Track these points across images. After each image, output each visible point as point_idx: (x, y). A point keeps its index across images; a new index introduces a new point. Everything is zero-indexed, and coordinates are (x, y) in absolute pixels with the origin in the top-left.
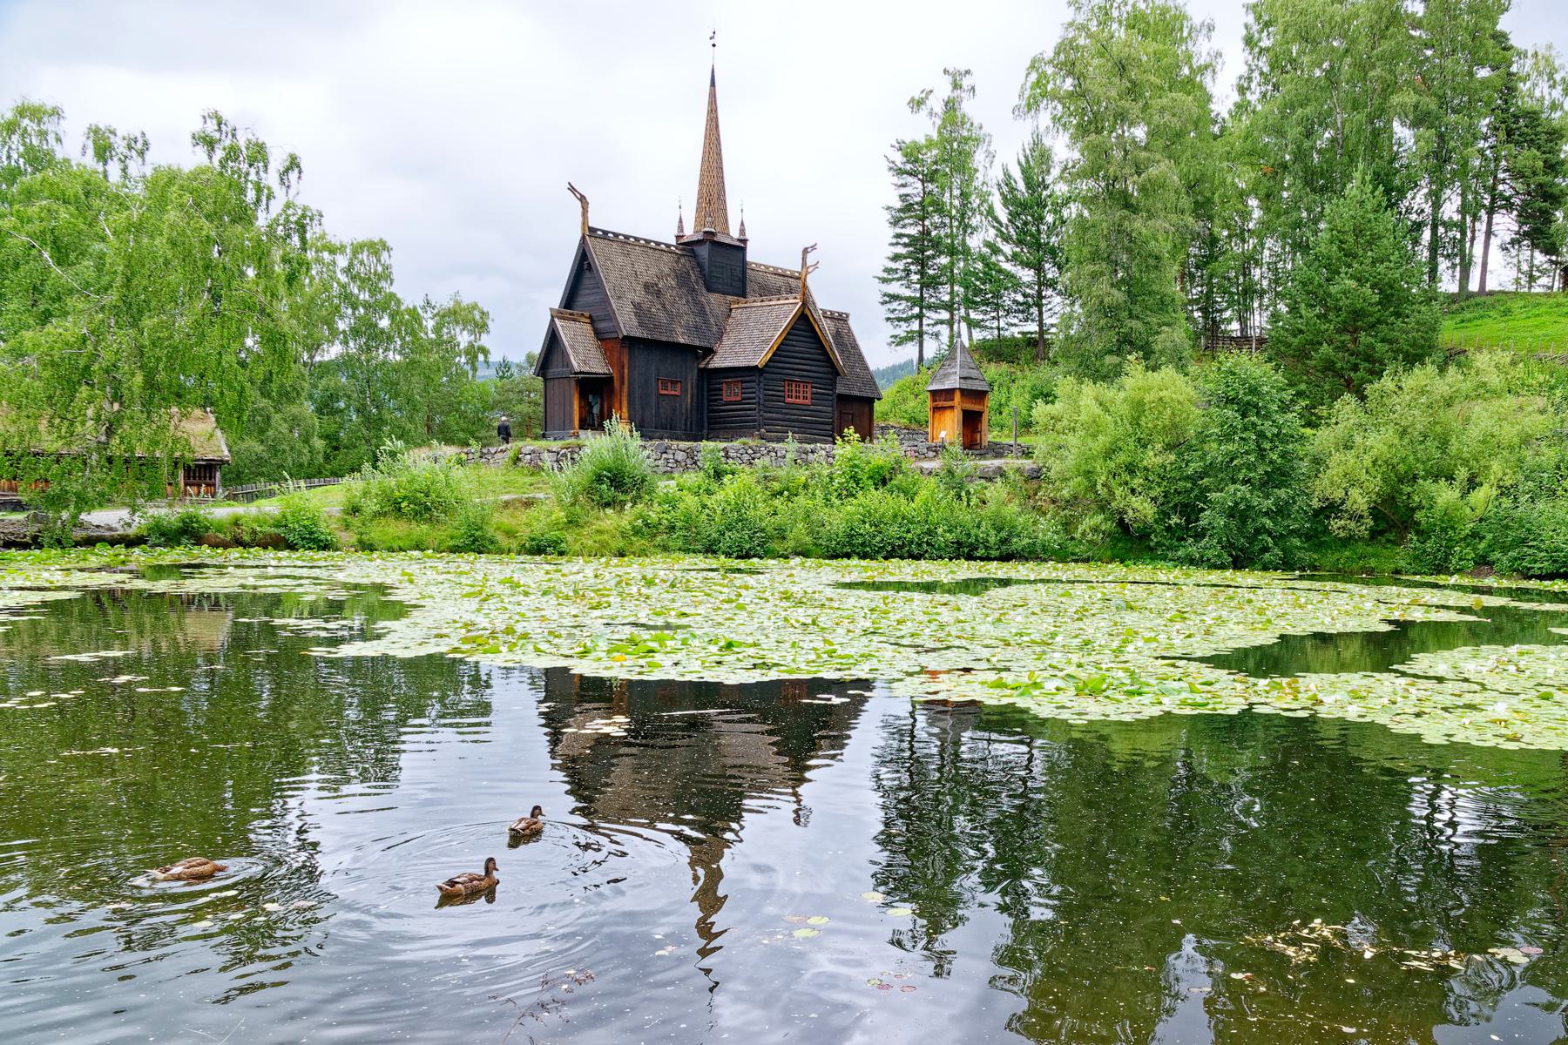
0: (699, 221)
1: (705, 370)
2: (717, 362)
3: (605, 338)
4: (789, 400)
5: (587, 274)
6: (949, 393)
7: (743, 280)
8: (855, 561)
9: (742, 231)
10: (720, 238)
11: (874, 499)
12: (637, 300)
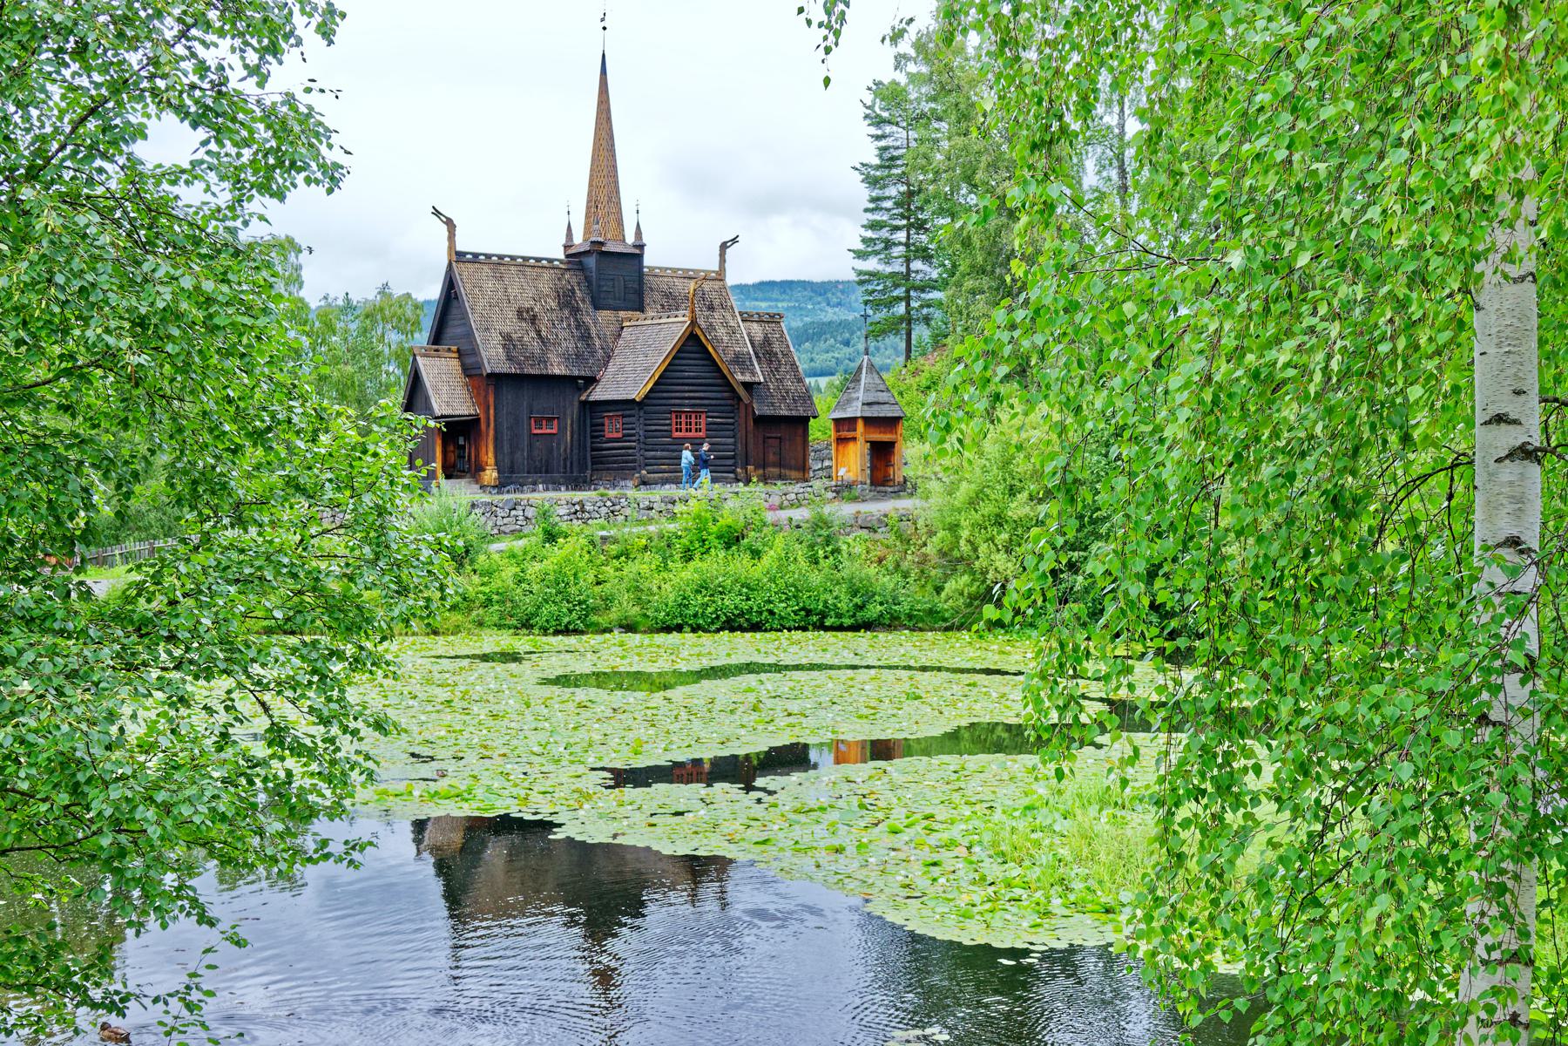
0: (588, 230)
1: (586, 403)
2: (599, 394)
3: (471, 370)
5: (455, 303)
7: (640, 293)
8: (688, 637)
11: (715, 565)
12: (507, 329)
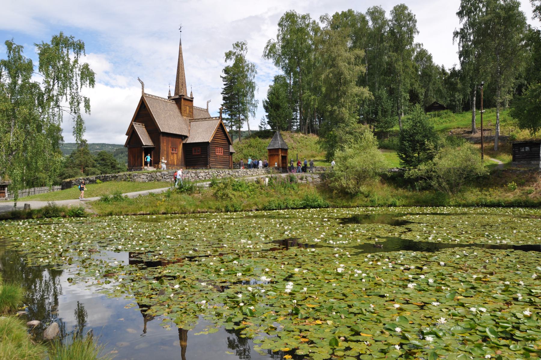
2: (189, 141)
4: (217, 154)
6: (277, 150)
9: (191, 95)
10: (185, 97)
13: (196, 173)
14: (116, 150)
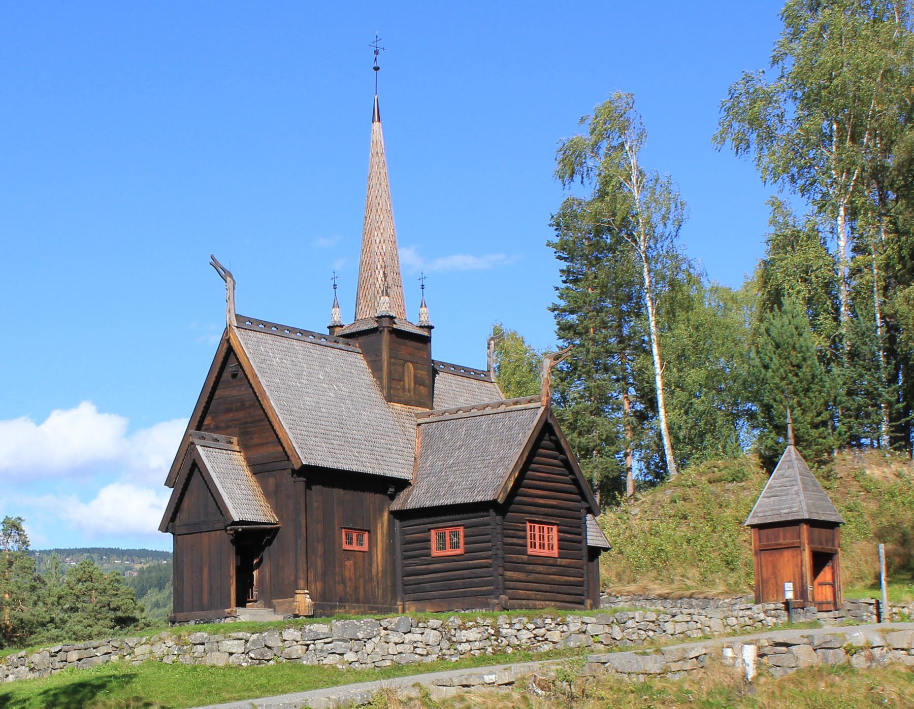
4: (530, 551)
13: (442, 629)
14: (142, 571)
